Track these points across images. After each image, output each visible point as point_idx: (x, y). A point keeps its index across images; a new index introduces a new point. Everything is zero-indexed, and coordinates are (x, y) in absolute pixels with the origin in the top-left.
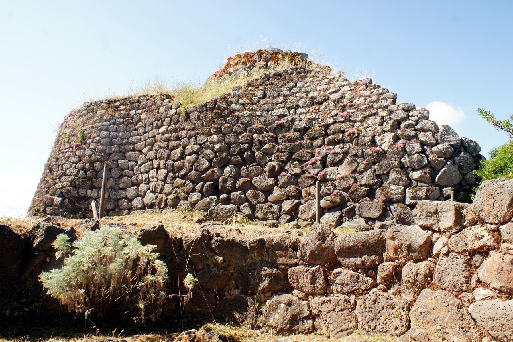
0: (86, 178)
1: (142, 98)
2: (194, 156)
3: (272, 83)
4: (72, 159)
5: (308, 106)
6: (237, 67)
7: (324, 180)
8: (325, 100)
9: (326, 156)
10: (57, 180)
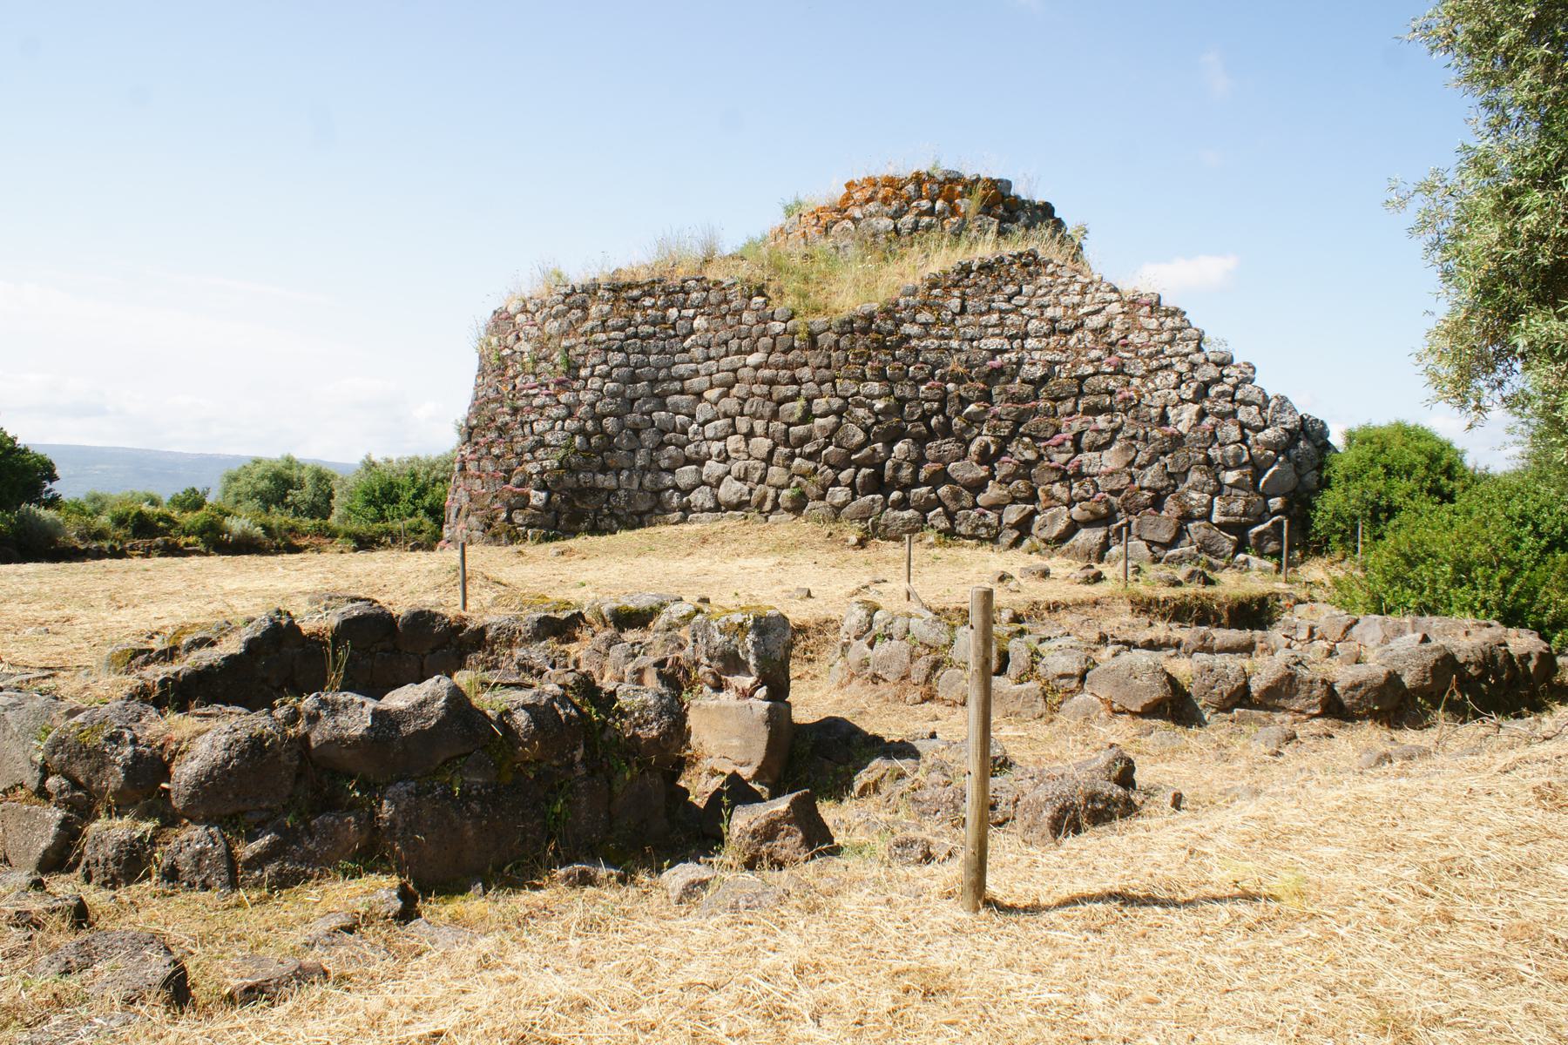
0: (587, 451)
1: (692, 283)
2: (832, 419)
3: (976, 284)
4: (554, 412)
5: (1046, 336)
6: (872, 207)
7: (1079, 475)
8: (1076, 327)
9: (1081, 433)
10: (528, 456)
